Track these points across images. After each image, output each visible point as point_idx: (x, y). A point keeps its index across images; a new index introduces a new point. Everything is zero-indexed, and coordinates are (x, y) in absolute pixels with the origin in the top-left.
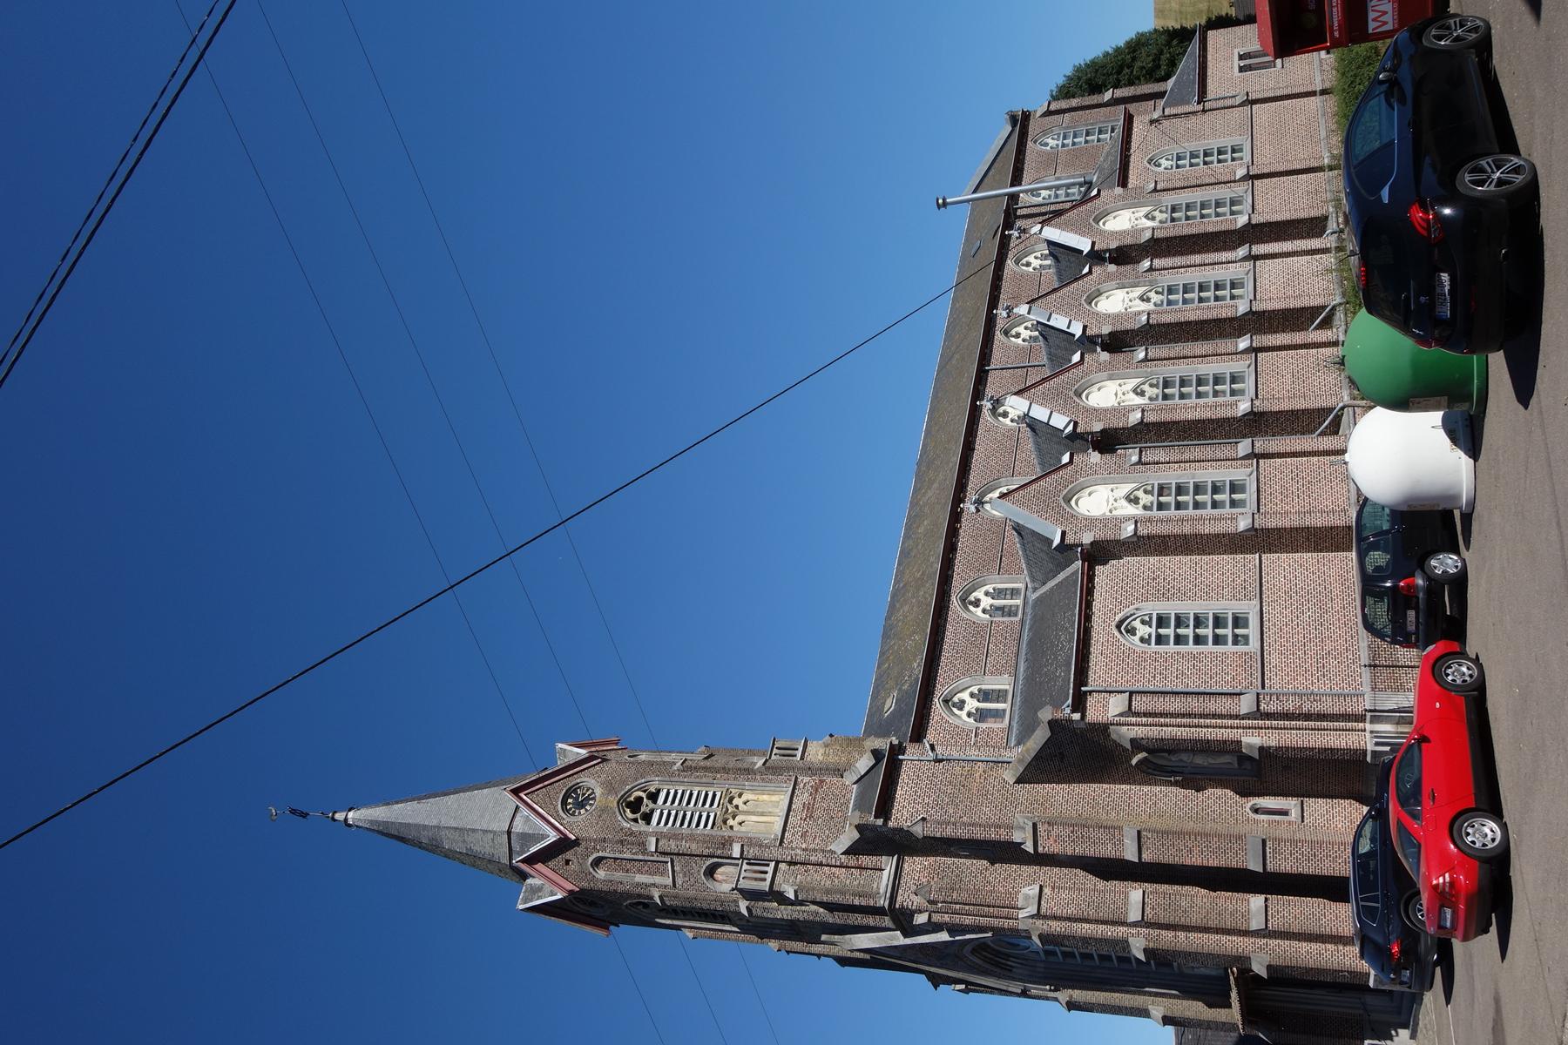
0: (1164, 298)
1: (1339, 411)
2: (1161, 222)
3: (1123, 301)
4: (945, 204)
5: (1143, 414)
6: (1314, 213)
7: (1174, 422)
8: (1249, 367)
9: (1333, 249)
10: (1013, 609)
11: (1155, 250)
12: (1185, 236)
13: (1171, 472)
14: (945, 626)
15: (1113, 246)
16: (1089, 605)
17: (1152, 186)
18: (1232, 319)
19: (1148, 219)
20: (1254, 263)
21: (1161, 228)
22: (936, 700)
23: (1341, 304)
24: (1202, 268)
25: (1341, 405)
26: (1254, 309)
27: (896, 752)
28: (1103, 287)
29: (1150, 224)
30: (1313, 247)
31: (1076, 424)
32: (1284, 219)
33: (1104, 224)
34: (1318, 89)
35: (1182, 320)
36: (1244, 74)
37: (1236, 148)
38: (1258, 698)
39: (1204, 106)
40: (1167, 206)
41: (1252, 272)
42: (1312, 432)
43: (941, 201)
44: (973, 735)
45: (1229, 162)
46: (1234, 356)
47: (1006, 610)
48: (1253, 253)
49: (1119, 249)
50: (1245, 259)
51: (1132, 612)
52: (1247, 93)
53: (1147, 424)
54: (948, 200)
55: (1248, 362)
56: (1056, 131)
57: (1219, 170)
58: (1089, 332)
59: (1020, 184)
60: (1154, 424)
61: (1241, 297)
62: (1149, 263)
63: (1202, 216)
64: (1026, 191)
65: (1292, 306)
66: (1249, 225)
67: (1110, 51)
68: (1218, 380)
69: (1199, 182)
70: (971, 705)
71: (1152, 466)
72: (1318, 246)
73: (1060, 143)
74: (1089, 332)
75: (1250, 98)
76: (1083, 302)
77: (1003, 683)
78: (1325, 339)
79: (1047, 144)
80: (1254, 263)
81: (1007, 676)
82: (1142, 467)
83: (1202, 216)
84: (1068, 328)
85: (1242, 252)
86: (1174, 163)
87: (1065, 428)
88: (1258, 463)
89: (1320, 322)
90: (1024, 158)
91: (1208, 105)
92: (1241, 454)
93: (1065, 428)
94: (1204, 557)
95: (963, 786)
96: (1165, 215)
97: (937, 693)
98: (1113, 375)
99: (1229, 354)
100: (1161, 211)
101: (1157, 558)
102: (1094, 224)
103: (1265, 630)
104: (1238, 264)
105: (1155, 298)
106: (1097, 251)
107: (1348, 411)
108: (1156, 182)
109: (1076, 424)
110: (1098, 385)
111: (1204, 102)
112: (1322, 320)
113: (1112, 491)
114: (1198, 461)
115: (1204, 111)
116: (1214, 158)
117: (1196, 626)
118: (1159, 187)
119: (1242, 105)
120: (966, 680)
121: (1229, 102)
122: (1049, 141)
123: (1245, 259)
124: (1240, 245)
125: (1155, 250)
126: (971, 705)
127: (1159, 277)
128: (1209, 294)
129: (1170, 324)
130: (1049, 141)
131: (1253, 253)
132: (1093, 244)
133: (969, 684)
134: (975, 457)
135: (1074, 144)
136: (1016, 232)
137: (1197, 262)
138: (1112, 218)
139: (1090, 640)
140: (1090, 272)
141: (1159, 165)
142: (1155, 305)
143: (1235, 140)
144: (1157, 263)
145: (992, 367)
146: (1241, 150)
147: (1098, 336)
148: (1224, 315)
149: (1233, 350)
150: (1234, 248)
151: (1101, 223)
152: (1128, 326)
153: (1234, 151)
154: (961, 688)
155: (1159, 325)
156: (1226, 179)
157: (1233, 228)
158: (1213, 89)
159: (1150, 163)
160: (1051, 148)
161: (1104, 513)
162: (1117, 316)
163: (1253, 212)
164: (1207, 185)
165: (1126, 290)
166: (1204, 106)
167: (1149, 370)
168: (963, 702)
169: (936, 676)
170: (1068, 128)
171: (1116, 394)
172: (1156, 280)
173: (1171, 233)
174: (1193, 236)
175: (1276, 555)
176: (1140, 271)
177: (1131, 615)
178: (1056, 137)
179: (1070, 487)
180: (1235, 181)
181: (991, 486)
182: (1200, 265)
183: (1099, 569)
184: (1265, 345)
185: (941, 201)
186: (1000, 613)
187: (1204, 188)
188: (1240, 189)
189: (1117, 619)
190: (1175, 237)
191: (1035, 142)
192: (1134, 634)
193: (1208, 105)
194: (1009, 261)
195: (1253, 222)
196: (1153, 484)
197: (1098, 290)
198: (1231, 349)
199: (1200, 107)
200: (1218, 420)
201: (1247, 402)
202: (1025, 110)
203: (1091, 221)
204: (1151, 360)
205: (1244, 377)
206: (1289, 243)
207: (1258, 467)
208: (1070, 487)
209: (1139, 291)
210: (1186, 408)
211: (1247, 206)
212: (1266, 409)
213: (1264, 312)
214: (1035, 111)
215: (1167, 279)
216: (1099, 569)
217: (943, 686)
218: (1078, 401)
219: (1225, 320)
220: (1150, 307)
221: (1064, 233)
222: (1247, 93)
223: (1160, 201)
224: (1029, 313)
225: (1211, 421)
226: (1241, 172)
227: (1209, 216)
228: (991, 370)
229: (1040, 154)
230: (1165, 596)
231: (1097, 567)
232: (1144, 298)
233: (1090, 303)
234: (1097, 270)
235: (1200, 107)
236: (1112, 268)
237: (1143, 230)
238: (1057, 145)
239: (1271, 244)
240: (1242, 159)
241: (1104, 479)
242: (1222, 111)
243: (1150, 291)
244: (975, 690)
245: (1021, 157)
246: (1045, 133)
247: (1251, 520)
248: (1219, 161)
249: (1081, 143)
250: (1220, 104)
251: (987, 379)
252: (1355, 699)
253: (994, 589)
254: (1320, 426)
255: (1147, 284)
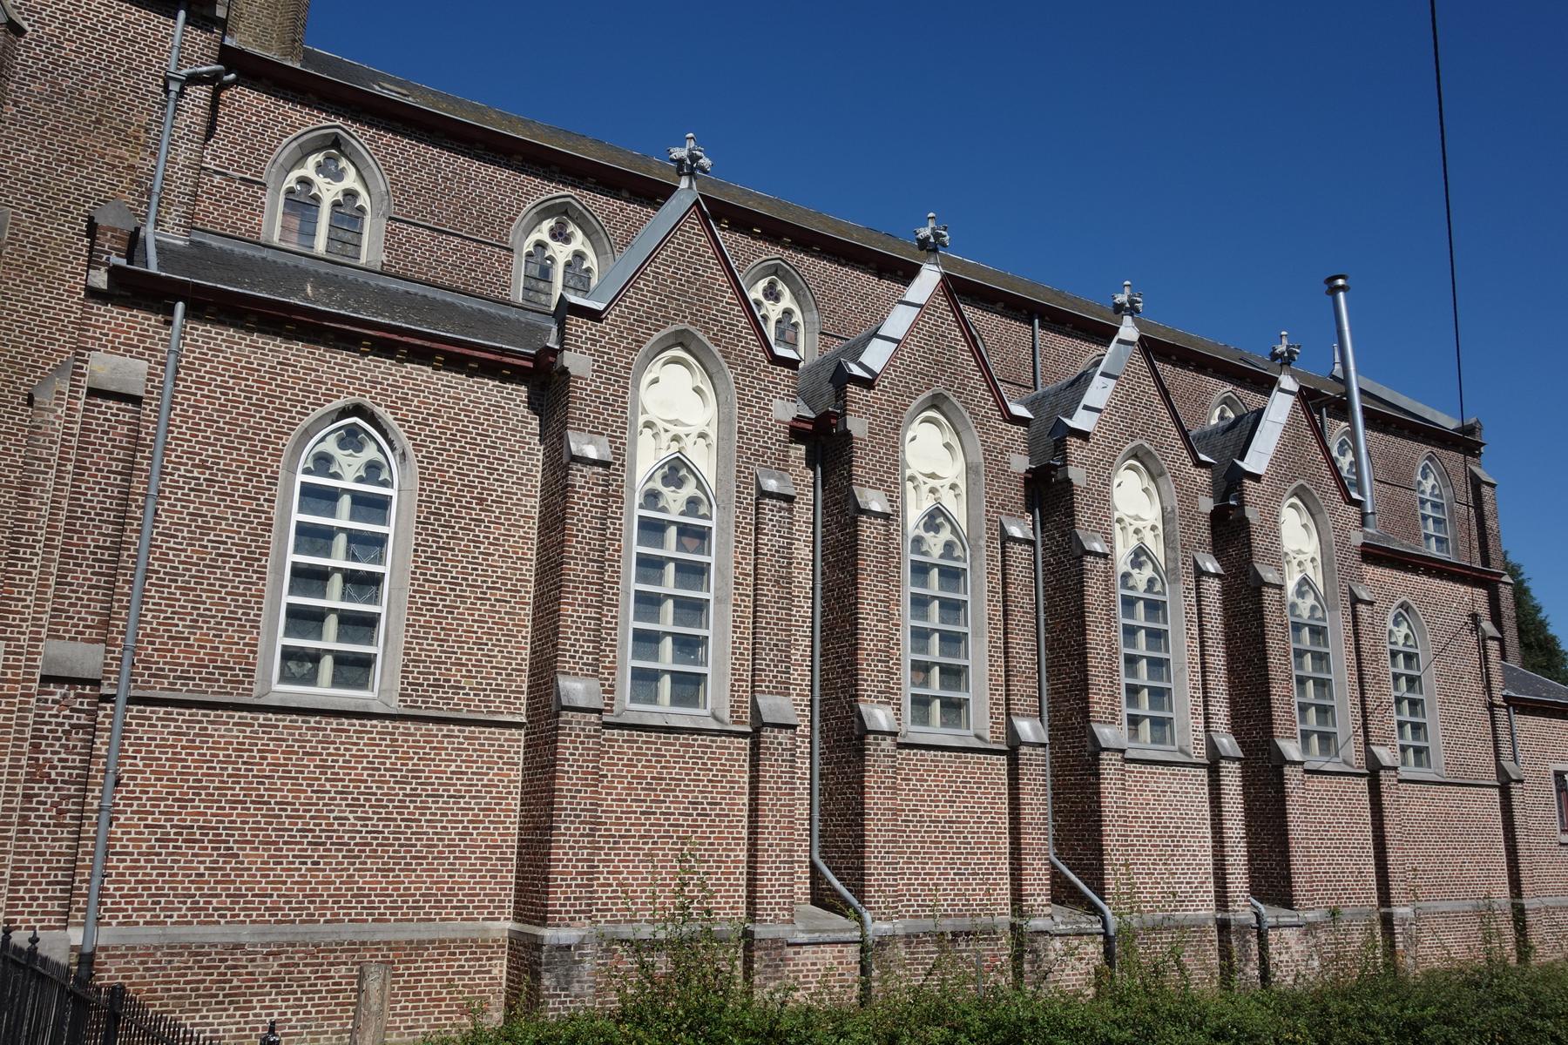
0: (1140, 592)
1: (856, 911)
2: (1294, 606)
3: (1138, 518)
4: (1334, 290)
5: (877, 515)
6: (1300, 882)
7: (855, 577)
8: (978, 737)
9: (1225, 915)
10: (543, 298)
11: (1238, 591)
12: (1264, 642)
13: (732, 556)
14: (508, 167)
15: (1251, 513)
16: (421, 355)
17: (1364, 596)
18: (1085, 712)
19: (1300, 585)
20: (1202, 766)
21: (1281, 601)
22: (338, 123)
23: (1105, 926)
24: (1198, 668)
25: (868, 916)
26: (1104, 755)
27: (194, 8)
28: (1168, 484)
29: (1291, 585)
30: (1230, 878)
31: (868, 384)
32: (1291, 826)
33: (1292, 506)
34: (1524, 901)
35: (1089, 618)
36: (1552, 778)
37: (1424, 756)
38: (84, 682)
39: (1500, 706)
40: (1325, 620)
41: (1183, 758)
42: (1059, 856)
43: (1340, 282)
44: (248, 176)
45: (1399, 742)
46: (1003, 709)
47: (542, 285)
48: (1223, 763)
49: (1244, 523)
50: (1212, 747)
51: (397, 444)
52: (1521, 781)
53: (855, 522)
54: (1341, 295)
55: (988, 736)
56: (1445, 493)
57: (1387, 720)
58: (1073, 443)
59: (1367, 426)
60: (855, 536)
61: (1134, 735)
62: (1212, 570)
63: (1301, 681)
64: (1353, 434)
65: (1107, 829)
66: (1282, 761)
67: (1542, 615)
68: (953, 674)
69: (1368, 679)
70: (329, 191)
71: (751, 519)
72: (1231, 888)
73: (1427, 496)
74: (1073, 443)
75: (1513, 785)
76: (1138, 442)
77: (371, 250)
78: (1027, 889)
79: (1425, 476)
80: (1202, 766)
81: (385, 259)
82: (751, 500)
83: (1301, 681)
84: (1086, 408)
85: (1227, 743)
86: (1400, 647)
87: (862, 366)
88: (743, 735)
89: (1070, 882)
90: (1404, 437)
91: (1501, 714)
92: (762, 701)
93: (862, 366)
94: (529, 610)
95: (98, 121)
96: (1306, 614)
97: (354, 128)
98: (977, 473)
99: (1007, 699)
100: (1313, 608)
101: (536, 513)
102: (1295, 485)
103: (312, 720)
104: (1202, 736)
105: (1141, 577)
106: (1241, 484)
107: (851, 930)
108: (1371, 603)
109: (868, 384)
110: (955, 443)
111: (1507, 708)
112: (1075, 887)
113: (702, 435)
114: (755, 612)
115: (1491, 706)
116: (1406, 717)
117: (677, 677)
118: (1361, 607)
119: (1501, 771)
120: (381, 184)
121: (1506, 750)
122: (1431, 482)
123: (1212, 747)
124: (1242, 744)
125: (1238, 591)
126: (329, 191)
127: (1182, 588)
128: (1143, 676)
129: (1081, 594)
130: (1431, 482)
131: (1223, 763)
132: (1256, 478)
133: (372, 191)
134: (864, 277)
135: (1425, 518)
136: (1284, 348)
137: (1210, 659)
138: (1305, 521)
139: (326, 344)
140: (1199, 464)
141: (1396, 623)
142: (1126, 576)
143: (1438, 756)
144: (1213, 587)
145: (1039, 332)
146: (1418, 763)
147: (1065, 460)
148: (1096, 698)
149: (1015, 708)
150: (1236, 730)
151: (1295, 500)
152: (1083, 517)
153: (1418, 751)
154: (365, 174)
155: (1081, 573)
156: (1372, 727)
157: (1277, 731)
158: (1528, 725)
159: (1401, 606)
160: (1420, 483)
161: (645, 411)
162: (1105, 499)
163: (1307, 771)
164: (1363, 694)
165: (1160, 527)
166: (1500, 706)
167: (983, 543)
168: (338, 176)
169: (395, 133)
170: (1452, 512)
171: (933, 476)
172: (1177, 580)
173: (1271, 618)
174: (1264, 659)
175: (519, 759)
176: (1196, 554)
177: (390, 443)
178: (1437, 492)
179: (715, 350)
180: (1367, 743)
181: (805, 295)
182: (1203, 664)
183: (520, 393)
184: (1023, 770)
185: (1340, 282)
186: (536, 273)
187: (1357, 687)
188: (1351, 752)
189: (380, 411)
190: (1262, 625)
191: (1429, 458)
192: (342, 444)
193: (1501, 714)
194: (1230, 387)
195: (1287, 770)
196: (711, 519)
197: (1162, 474)
198: (1018, 704)
199: (1498, 700)
200: (854, 663)
201: (889, 725)
202: (1482, 449)
203: (1302, 482)
204: (1003, 547)
205: (958, 726)
206: (1242, 833)
207: (730, 733)
208: (715, 350)
209: (1156, 548)
210: (889, 602)
211: (1316, 760)
212: (869, 761)
213: (1097, 775)
214: (1479, 465)
215: (1178, 600)
216: (521, 392)
217: (371, 140)
218: (921, 398)
219: (1086, 700)
220: (1122, 561)
221: (1279, 430)
222: (1521, 781)
223: (1334, 608)
224: (1120, 341)
225: (854, 649)
226: (1385, 755)
227: (1302, 692)
228: (1033, 330)
229: (1410, 463)
230: (431, 518)
231: (523, 388)
232: (1140, 555)
233: (1135, 457)
234: (1203, 477)
235: (1498, 700)
236: (1207, 505)
237: (1280, 570)
238: (1423, 492)
239: (1240, 799)
240: (1404, 764)
241: (730, 419)
242: (1490, 737)
243: (1155, 569)
244: (364, 200)
245: (1406, 432)
246: (1445, 475)
247: (581, 704)
248: (1401, 725)
249: (1426, 528)
250: (1504, 735)
251: (1016, 320)
252: (54, 906)
253: (588, 270)
254: (832, 869)
255: (1171, 565)
